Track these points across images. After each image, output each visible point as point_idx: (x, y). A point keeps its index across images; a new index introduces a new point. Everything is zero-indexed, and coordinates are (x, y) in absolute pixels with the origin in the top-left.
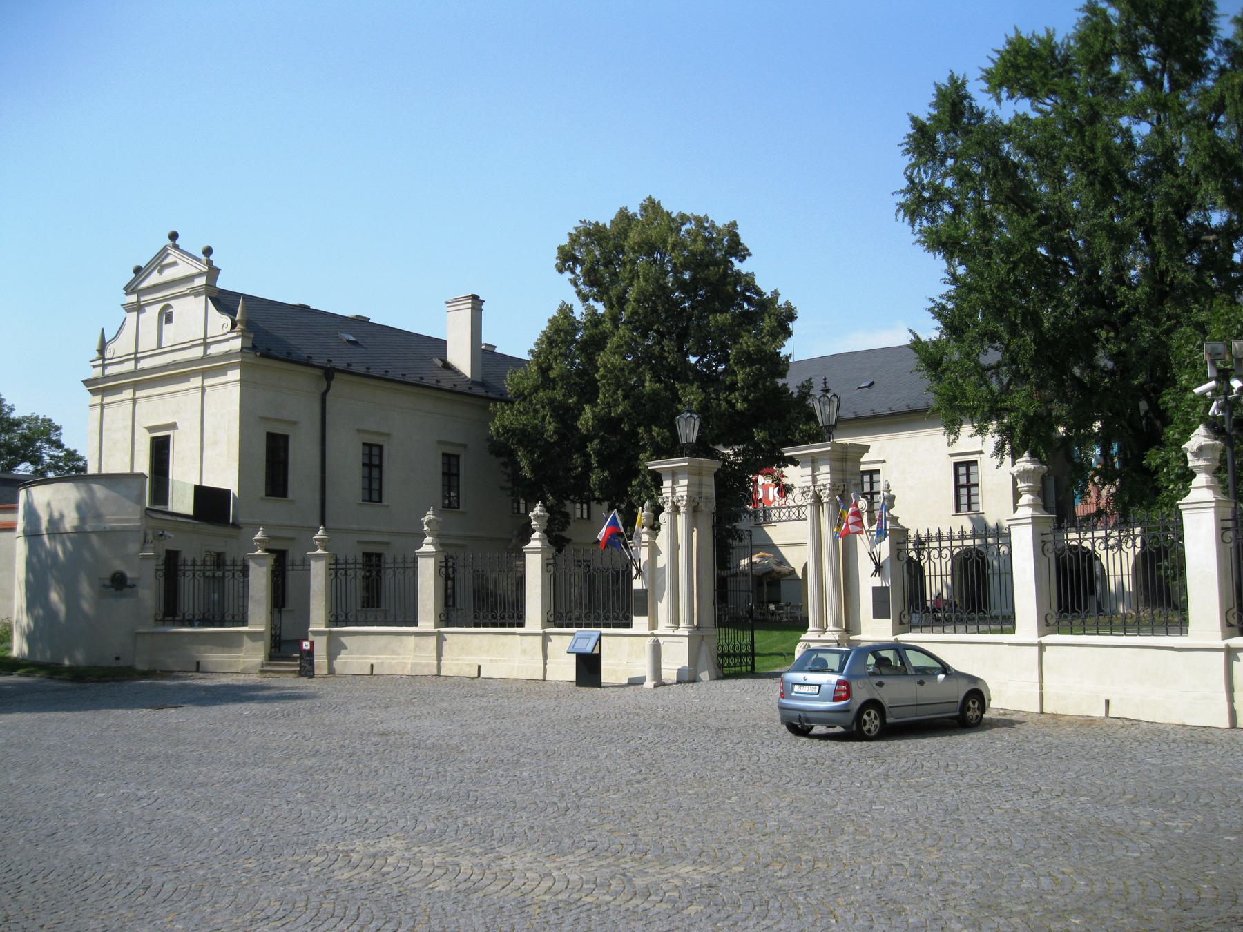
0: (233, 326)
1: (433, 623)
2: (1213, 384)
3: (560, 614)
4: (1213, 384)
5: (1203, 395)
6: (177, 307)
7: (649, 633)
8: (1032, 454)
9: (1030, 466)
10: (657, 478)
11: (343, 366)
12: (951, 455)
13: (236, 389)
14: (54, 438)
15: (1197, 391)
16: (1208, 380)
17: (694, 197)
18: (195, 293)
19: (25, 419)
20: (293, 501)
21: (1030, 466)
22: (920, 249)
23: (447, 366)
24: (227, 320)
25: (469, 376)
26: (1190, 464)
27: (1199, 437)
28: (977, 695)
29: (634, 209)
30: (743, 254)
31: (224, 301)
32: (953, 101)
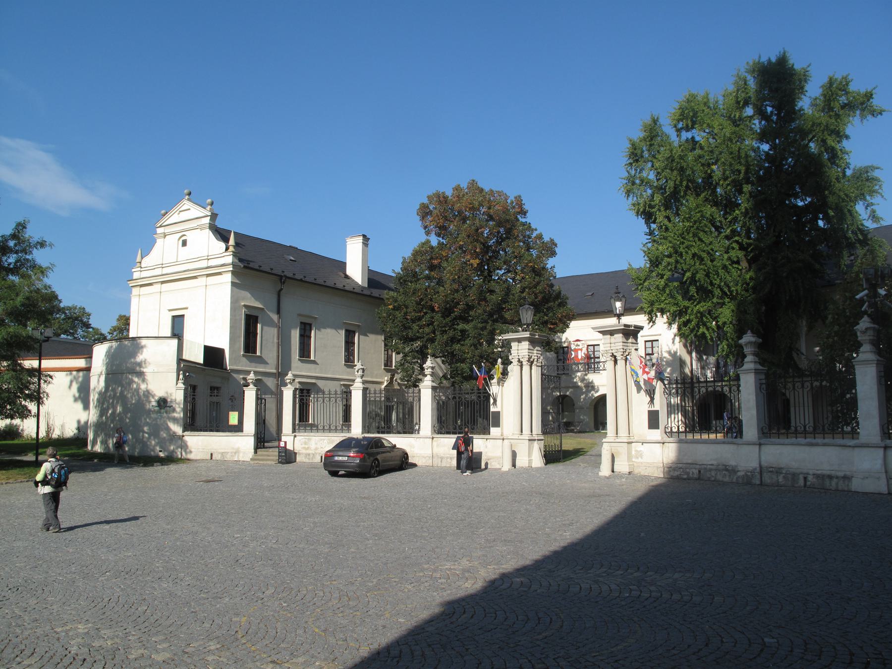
0: (227, 249)
1: (361, 430)
2: (866, 292)
3: (442, 426)
4: (866, 292)
5: (862, 298)
6: (190, 236)
7: (34, 420)
8: (753, 332)
9: (753, 339)
10: (507, 345)
11: (291, 275)
12: (170, 310)
13: (228, 288)
14: (85, 320)
15: (857, 297)
16: (864, 290)
17: (502, 181)
18: (201, 227)
19: (69, 308)
20: (314, 362)
21: (753, 339)
22: (632, 214)
23: (347, 277)
24: (222, 245)
25: (360, 283)
26: (859, 339)
27: (864, 323)
28: (405, 455)
29: (464, 185)
30: (524, 213)
31: (222, 235)
32: (653, 132)
